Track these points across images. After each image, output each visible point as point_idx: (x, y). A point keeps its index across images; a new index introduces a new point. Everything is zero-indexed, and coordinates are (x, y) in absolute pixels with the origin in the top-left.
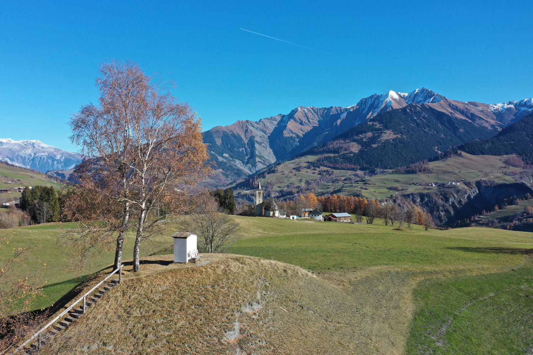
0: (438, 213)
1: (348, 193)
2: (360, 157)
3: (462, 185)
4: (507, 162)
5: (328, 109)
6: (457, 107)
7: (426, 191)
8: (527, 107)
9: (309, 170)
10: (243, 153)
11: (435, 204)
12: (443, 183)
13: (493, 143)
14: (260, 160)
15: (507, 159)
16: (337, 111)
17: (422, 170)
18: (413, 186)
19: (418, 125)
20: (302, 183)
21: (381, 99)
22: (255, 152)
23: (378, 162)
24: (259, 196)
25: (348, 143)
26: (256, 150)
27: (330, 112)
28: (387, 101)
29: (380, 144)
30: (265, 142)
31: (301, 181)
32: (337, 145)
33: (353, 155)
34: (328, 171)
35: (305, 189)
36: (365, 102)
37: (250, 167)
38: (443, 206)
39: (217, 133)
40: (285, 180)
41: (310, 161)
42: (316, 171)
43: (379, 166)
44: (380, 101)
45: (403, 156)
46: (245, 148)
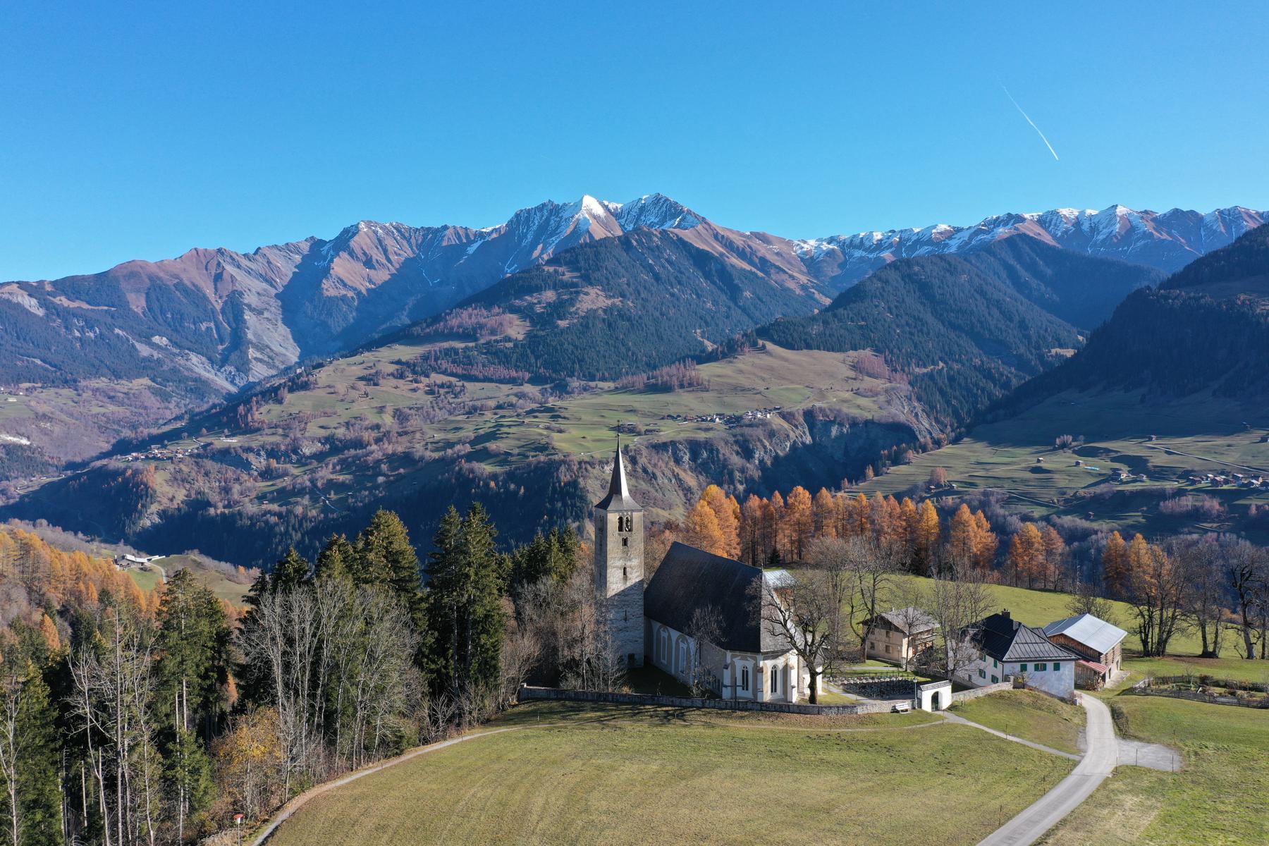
0: (732, 487)
1: (517, 442)
2: (529, 351)
3: (776, 419)
4: (855, 367)
5: (437, 230)
6: (731, 243)
7: (702, 436)
8: (865, 250)
9: (401, 381)
10: (211, 336)
11: (725, 466)
12: (736, 414)
13: (826, 323)
14: (258, 355)
15: (856, 360)
16: (459, 237)
17: (685, 384)
18: (670, 421)
19: (657, 278)
20: (384, 416)
21: (566, 215)
22: (246, 334)
23: (573, 364)
24: (625, 542)
25: (498, 314)
26: (248, 328)
27: (442, 240)
28: (578, 220)
29: (575, 321)
30: (273, 309)
31: (381, 410)
32: (470, 318)
33: (511, 345)
34: (450, 386)
35: (397, 433)
36: (528, 219)
37: (230, 372)
38: (742, 470)
39: (132, 280)
40: (340, 409)
41: (404, 360)
42: (420, 386)
43: (576, 374)
44: (561, 218)
45: (629, 350)
46: (215, 322)
